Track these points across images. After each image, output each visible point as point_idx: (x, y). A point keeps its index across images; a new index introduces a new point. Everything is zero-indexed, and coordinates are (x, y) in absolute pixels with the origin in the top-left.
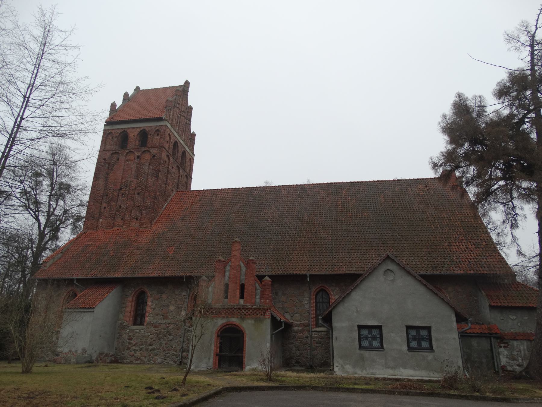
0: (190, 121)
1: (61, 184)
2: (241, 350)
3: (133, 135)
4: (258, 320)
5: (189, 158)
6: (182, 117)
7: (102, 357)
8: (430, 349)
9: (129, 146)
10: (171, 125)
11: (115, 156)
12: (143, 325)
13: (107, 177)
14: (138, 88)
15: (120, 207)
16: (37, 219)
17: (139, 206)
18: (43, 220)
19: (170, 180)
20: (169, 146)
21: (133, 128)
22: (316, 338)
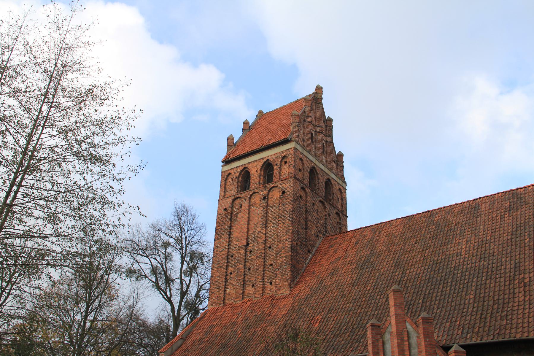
0: (331, 137)
3: (255, 171)
5: (337, 188)
6: (318, 134)
9: (252, 186)
10: (303, 147)
11: (238, 202)
13: (230, 232)
14: (261, 112)
15: (249, 269)
17: (272, 265)
18: (176, 299)
19: (313, 223)
21: (255, 161)
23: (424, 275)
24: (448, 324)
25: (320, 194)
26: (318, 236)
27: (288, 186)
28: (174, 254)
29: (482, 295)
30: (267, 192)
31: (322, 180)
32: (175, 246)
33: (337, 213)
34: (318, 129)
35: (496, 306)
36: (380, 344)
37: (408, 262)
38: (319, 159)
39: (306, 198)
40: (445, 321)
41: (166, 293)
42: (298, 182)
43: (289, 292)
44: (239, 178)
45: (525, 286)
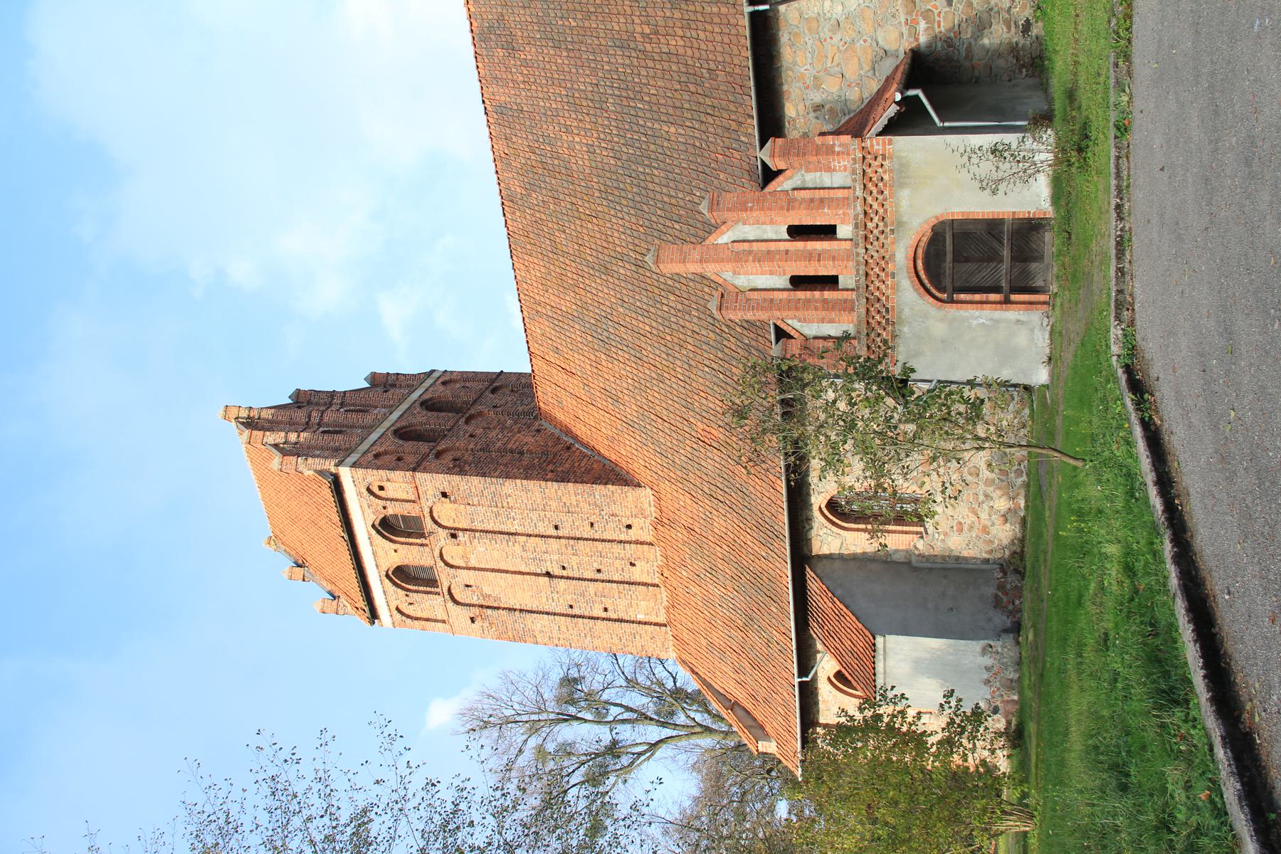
1: (559, 700)
2: (993, 226)
4: (903, 175)
5: (442, 388)
6: (326, 419)
7: (1005, 599)
10: (350, 451)
15: (599, 571)
16: (654, 746)
17: (592, 524)
23: (627, 218)
24: (722, 176)
25: (451, 423)
26: (538, 431)
27: (432, 483)
28: (560, 740)
29: (671, 111)
32: (544, 735)
35: (692, 88)
36: (755, 295)
37: (600, 249)
40: (716, 182)
41: (640, 754)
42: (426, 464)
43: (648, 490)
44: (408, 590)
45: (657, 33)
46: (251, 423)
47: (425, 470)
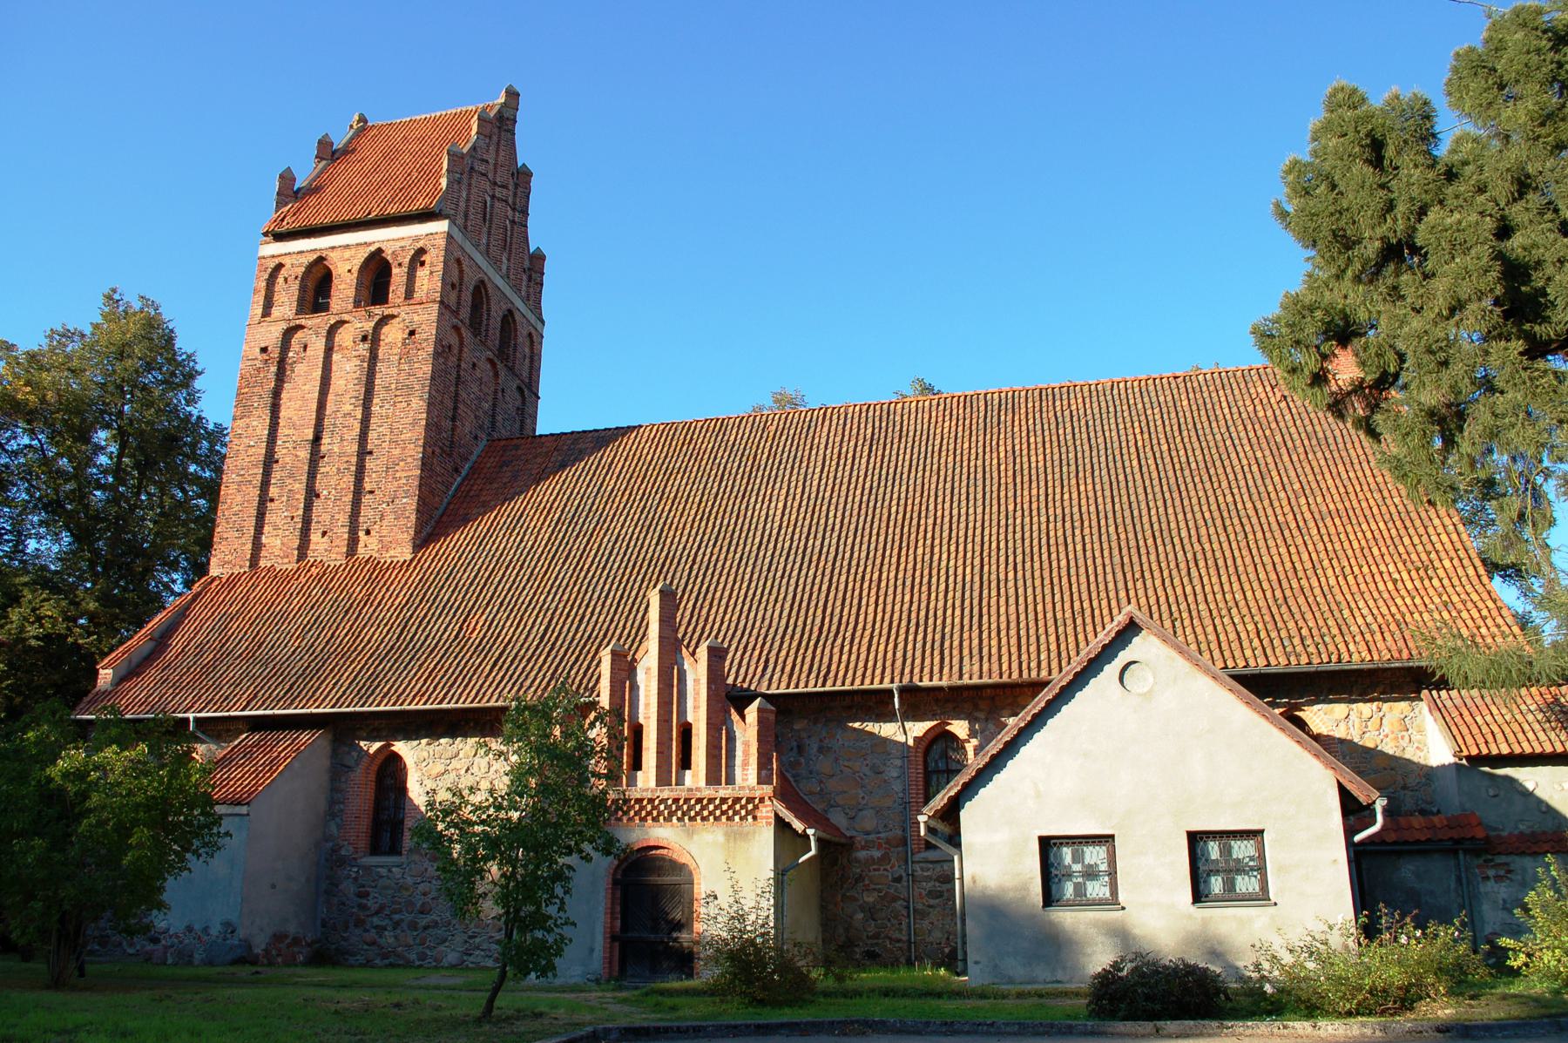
0: (525, 213)
5: (525, 333)
6: (497, 204)
8: (1262, 896)
10: (464, 229)
12: (400, 854)
20: (459, 297)
22: (928, 879)
26: (476, 437)
27: (426, 318)
30: (372, 324)
31: (497, 312)
33: (520, 389)
34: (499, 192)
38: (496, 263)
39: (461, 351)
42: (447, 315)
46: (500, 125)
47: (440, 314)
